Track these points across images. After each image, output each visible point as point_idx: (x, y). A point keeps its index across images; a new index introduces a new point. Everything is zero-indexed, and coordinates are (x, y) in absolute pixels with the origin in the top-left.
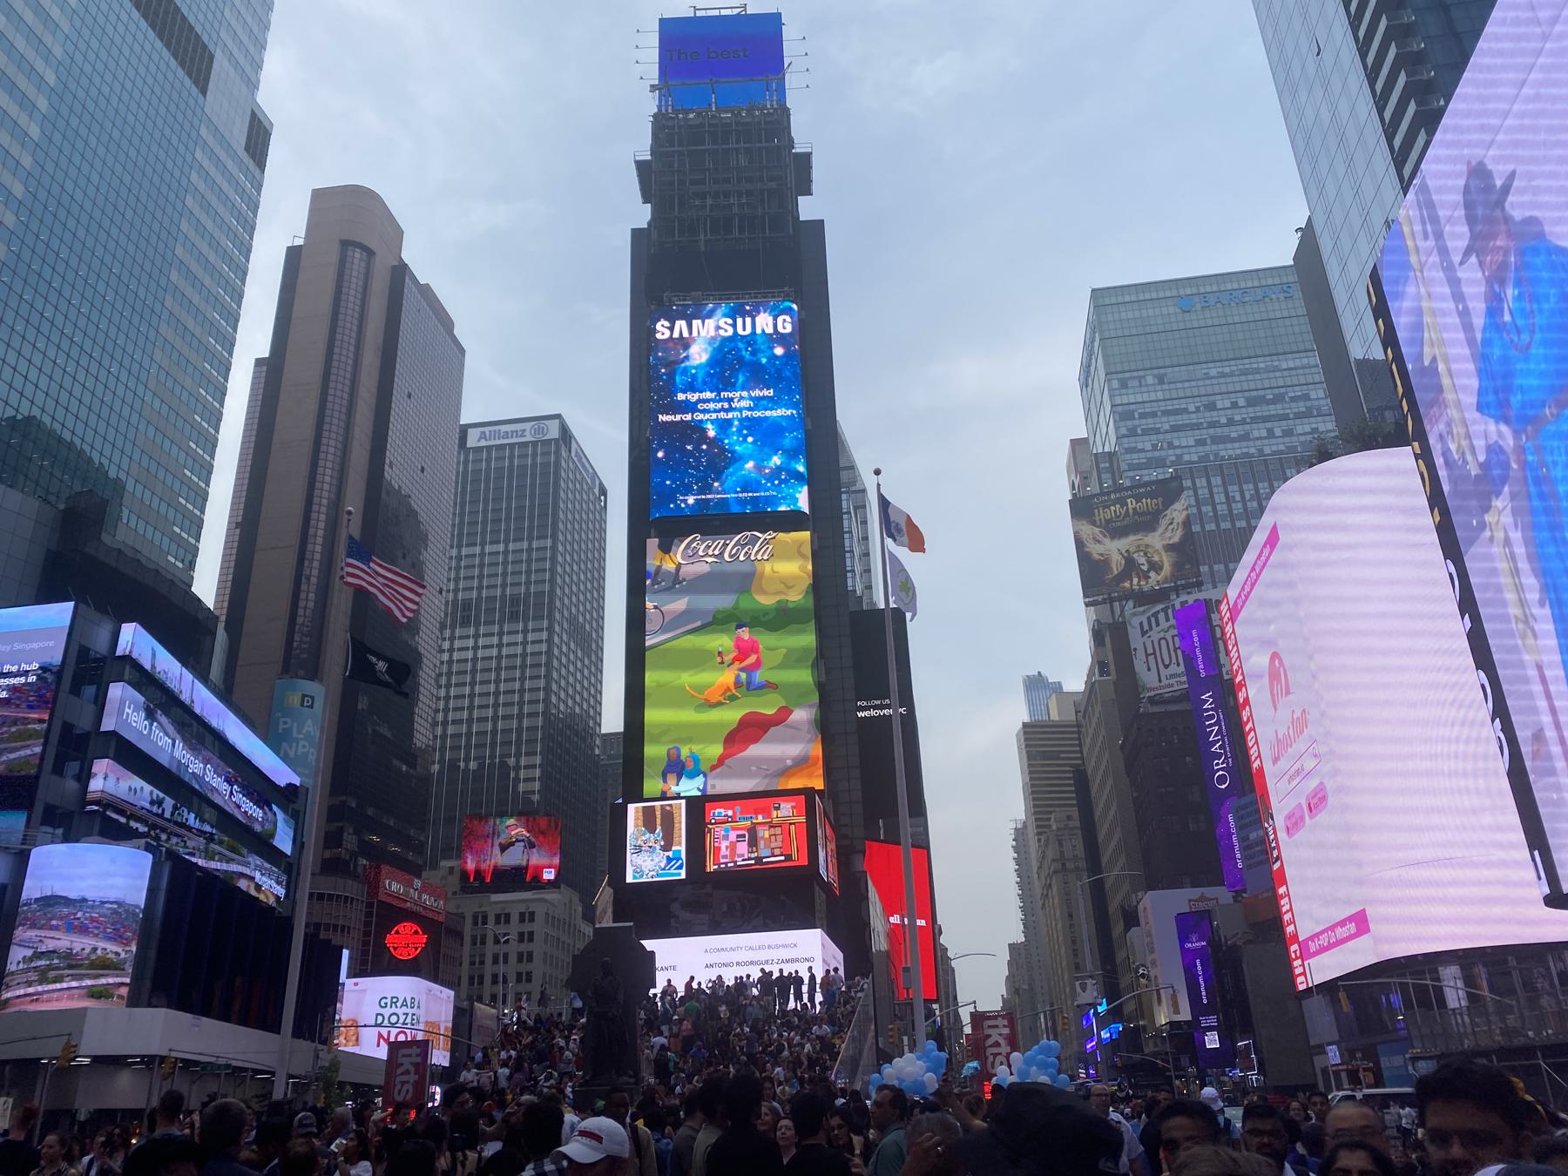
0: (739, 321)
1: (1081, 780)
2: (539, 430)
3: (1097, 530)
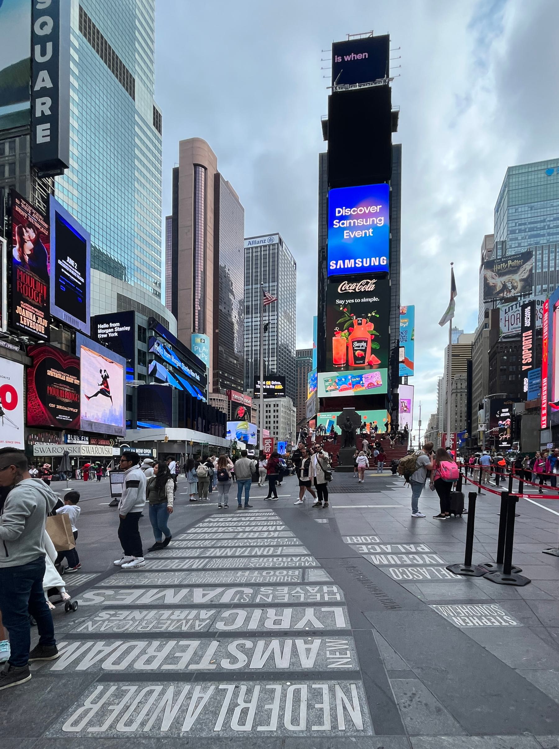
0: (365, 260)
1: (470, 364)
2: (271, 240)
3: (493, 274)
